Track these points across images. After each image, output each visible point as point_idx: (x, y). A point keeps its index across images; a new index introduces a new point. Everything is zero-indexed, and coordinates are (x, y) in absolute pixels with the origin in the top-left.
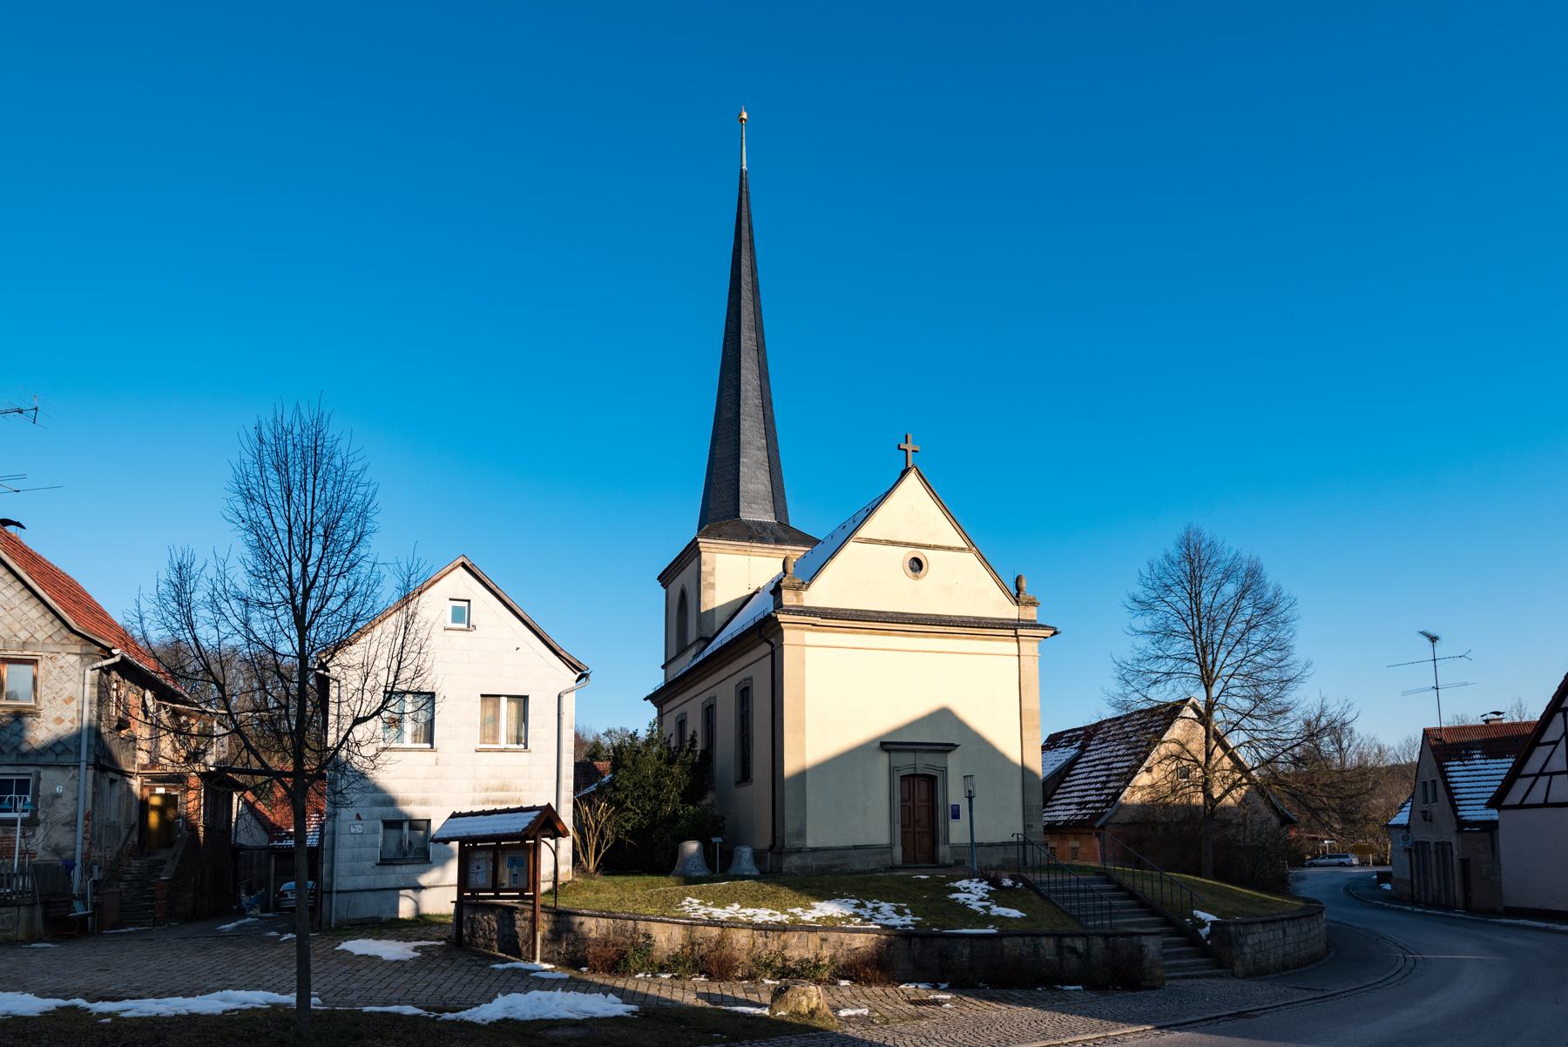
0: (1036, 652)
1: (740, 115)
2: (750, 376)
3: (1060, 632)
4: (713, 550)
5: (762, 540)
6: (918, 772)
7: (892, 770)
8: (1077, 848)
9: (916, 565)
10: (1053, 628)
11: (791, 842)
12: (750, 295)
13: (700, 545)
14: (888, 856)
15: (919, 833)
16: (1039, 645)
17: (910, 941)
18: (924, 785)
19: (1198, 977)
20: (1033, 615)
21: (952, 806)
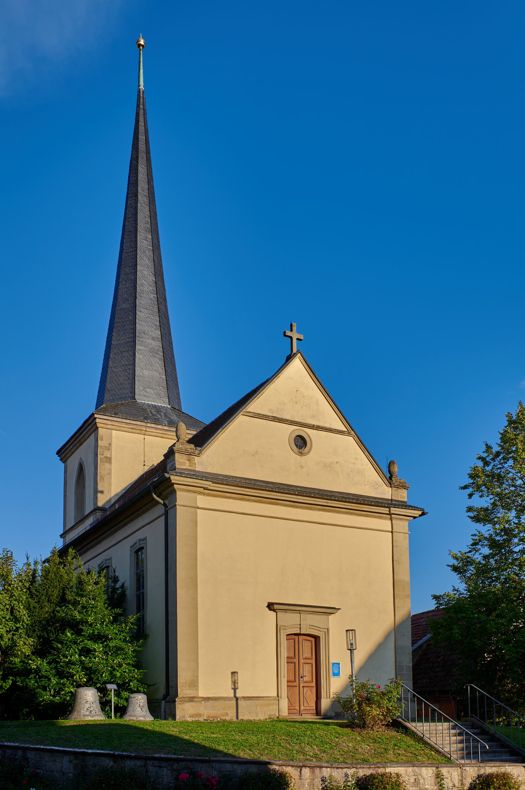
0: (406, 530)
1: (138, 41)
2: (146, 273)
3: (427, 513)
4: (109, 427)
5: (156, 421)
10: (421, 509)
12: (146, 200)
13: (97, 420)
16: (411, 527)
20: (404, 498)
21: (333, 664)
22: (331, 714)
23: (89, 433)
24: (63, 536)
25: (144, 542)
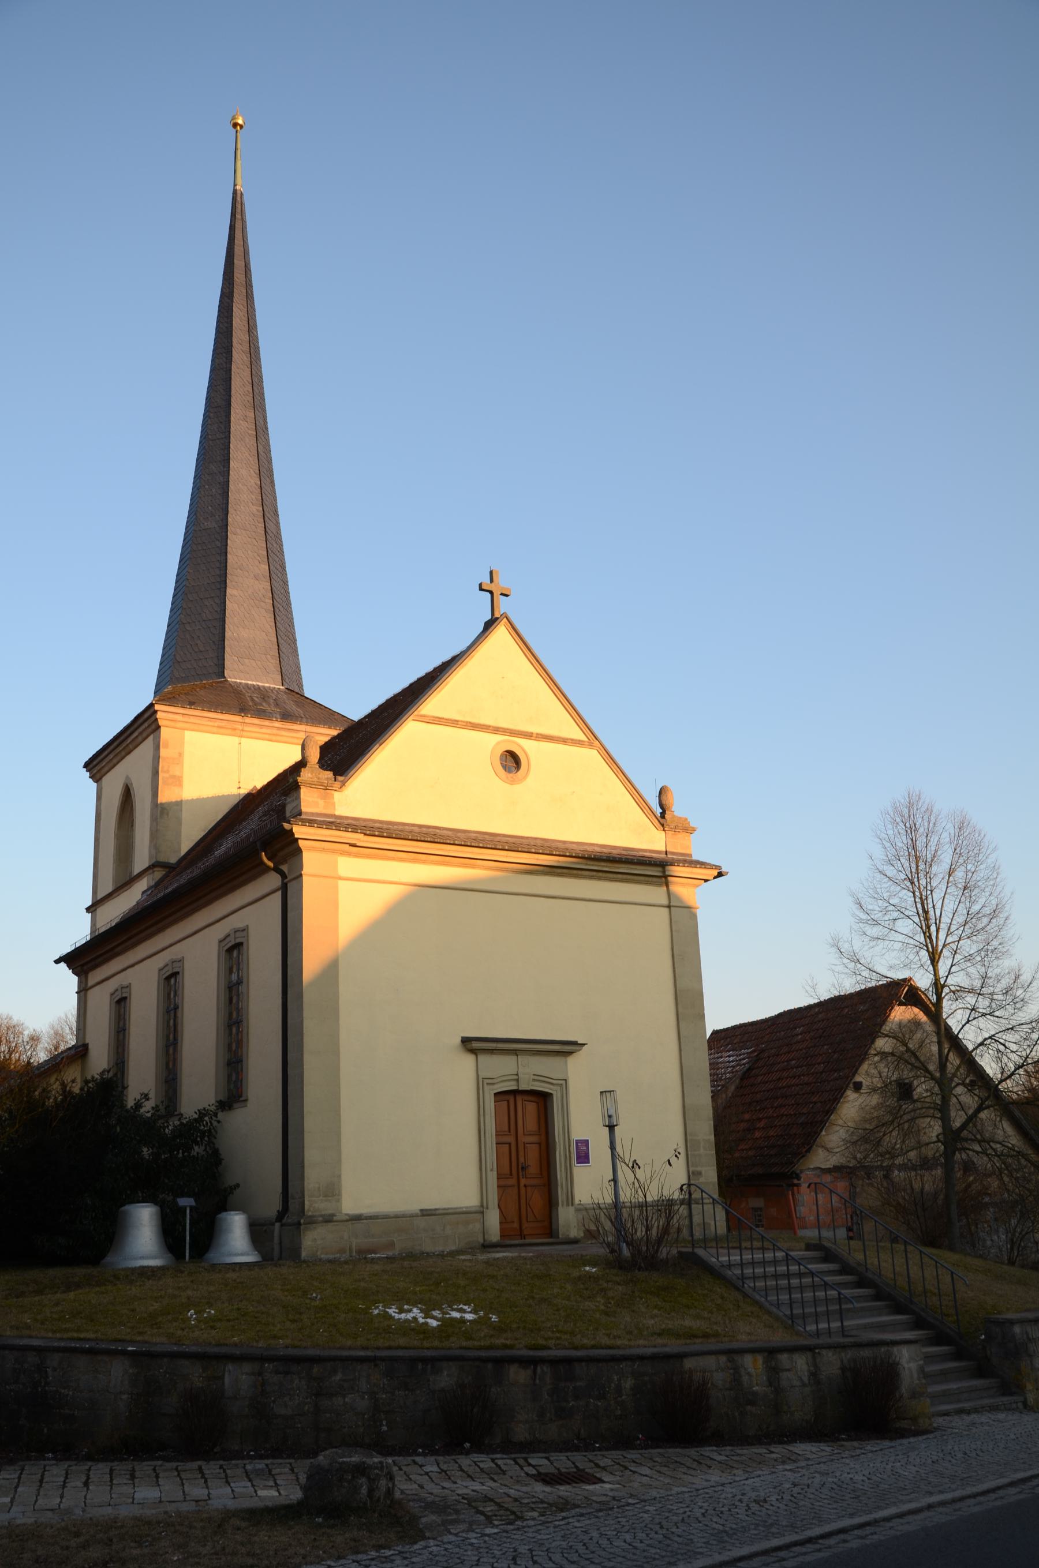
3: (727, 873)
5: (261, 714)
6: (523, 1087)
7: (481, 1083)
8: (760, 1209)
9: (511, 763)
10: (719, 867)
11: (316, 1205)
13: (159, 715)
14: (478, 1226)
18: (531, 1108)
19: (976, 1410)
21: (577, 1142)
22: (576, 1235)
23: (145, 735)
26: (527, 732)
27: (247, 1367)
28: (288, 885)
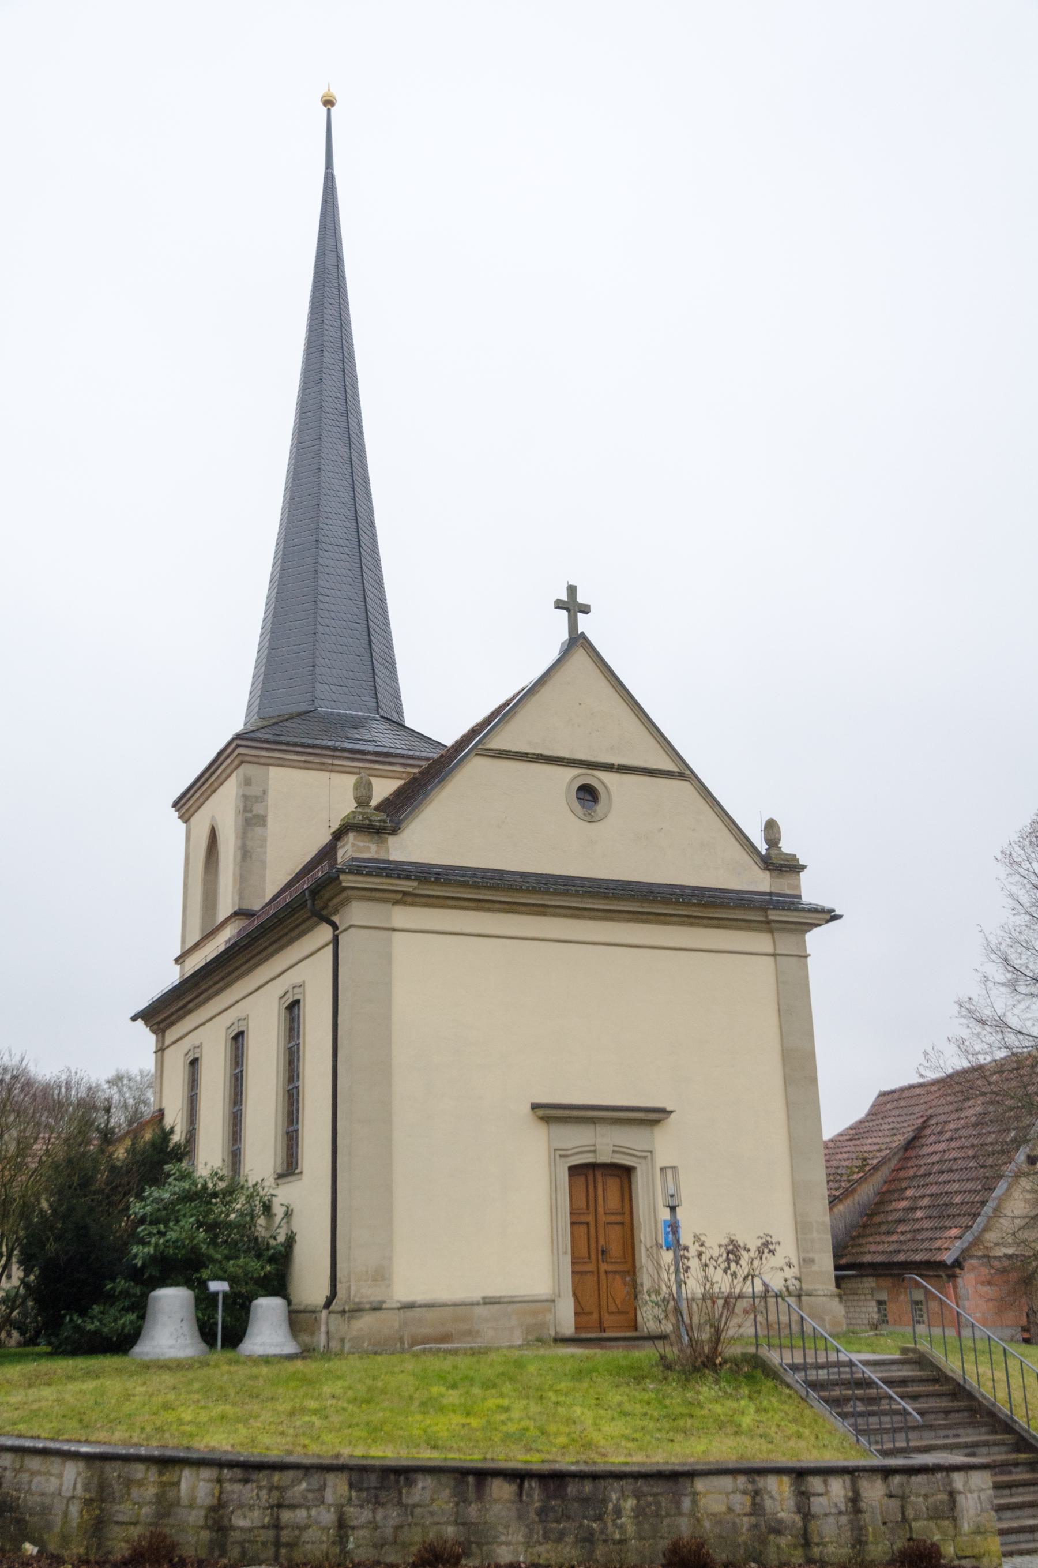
15: (606, 1272)
17: (521, 1487)
23: (228, 771)
24: (180, 961)
25: (301, 989)
26: (607, 764)
27: (206, 1473)
28: (340, 937)
